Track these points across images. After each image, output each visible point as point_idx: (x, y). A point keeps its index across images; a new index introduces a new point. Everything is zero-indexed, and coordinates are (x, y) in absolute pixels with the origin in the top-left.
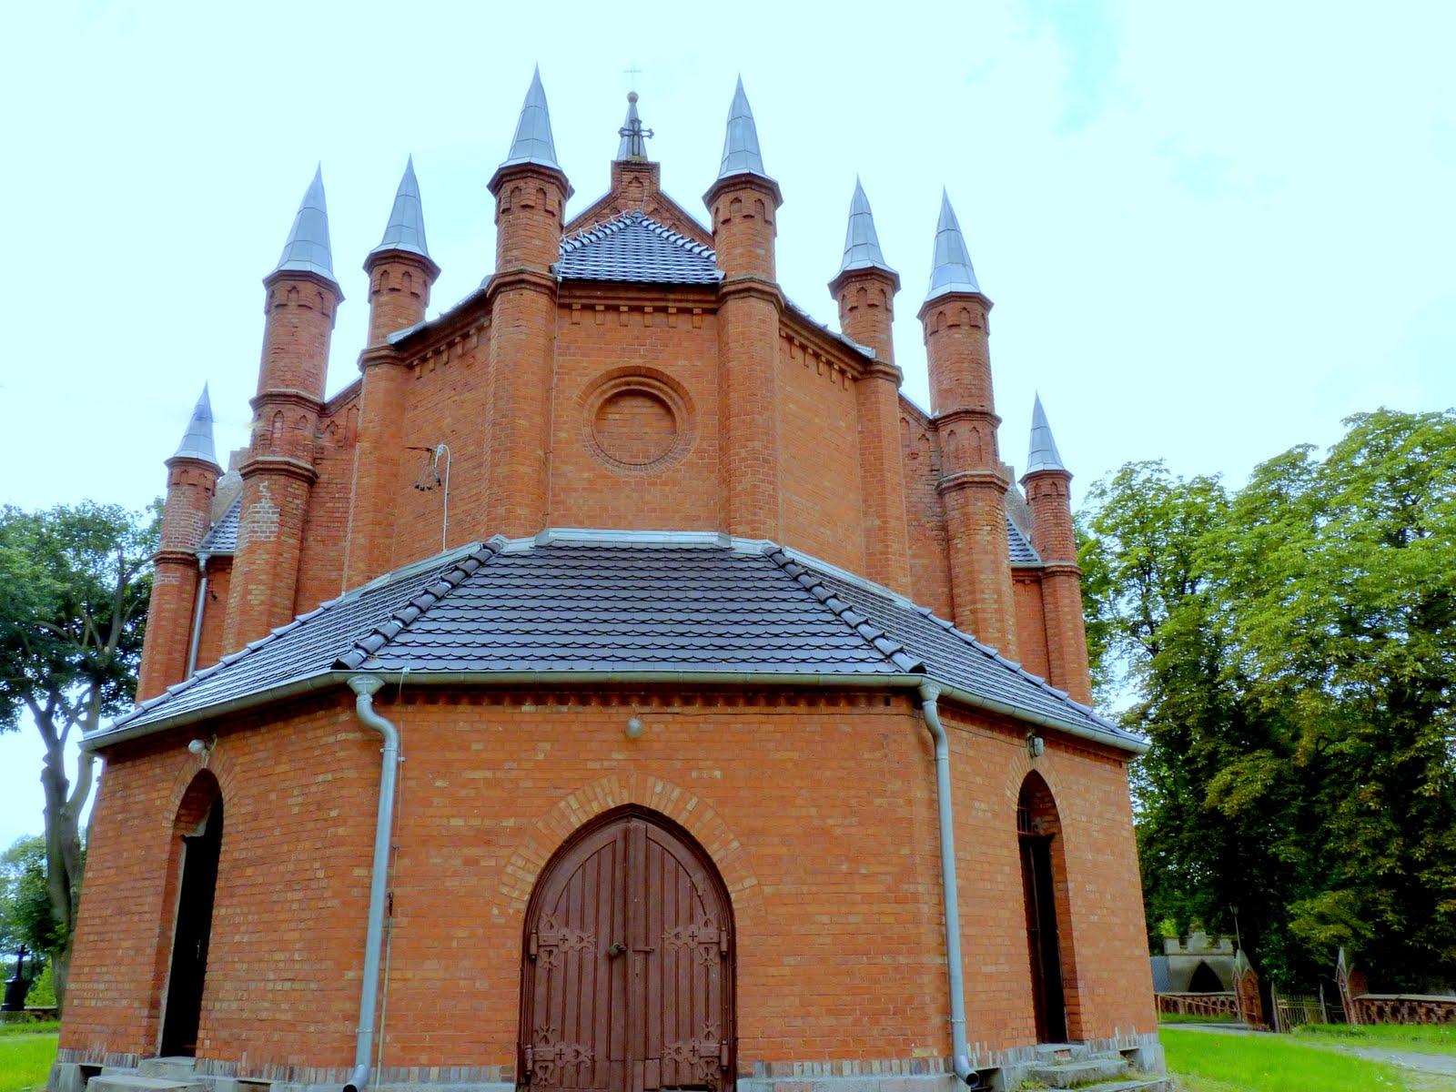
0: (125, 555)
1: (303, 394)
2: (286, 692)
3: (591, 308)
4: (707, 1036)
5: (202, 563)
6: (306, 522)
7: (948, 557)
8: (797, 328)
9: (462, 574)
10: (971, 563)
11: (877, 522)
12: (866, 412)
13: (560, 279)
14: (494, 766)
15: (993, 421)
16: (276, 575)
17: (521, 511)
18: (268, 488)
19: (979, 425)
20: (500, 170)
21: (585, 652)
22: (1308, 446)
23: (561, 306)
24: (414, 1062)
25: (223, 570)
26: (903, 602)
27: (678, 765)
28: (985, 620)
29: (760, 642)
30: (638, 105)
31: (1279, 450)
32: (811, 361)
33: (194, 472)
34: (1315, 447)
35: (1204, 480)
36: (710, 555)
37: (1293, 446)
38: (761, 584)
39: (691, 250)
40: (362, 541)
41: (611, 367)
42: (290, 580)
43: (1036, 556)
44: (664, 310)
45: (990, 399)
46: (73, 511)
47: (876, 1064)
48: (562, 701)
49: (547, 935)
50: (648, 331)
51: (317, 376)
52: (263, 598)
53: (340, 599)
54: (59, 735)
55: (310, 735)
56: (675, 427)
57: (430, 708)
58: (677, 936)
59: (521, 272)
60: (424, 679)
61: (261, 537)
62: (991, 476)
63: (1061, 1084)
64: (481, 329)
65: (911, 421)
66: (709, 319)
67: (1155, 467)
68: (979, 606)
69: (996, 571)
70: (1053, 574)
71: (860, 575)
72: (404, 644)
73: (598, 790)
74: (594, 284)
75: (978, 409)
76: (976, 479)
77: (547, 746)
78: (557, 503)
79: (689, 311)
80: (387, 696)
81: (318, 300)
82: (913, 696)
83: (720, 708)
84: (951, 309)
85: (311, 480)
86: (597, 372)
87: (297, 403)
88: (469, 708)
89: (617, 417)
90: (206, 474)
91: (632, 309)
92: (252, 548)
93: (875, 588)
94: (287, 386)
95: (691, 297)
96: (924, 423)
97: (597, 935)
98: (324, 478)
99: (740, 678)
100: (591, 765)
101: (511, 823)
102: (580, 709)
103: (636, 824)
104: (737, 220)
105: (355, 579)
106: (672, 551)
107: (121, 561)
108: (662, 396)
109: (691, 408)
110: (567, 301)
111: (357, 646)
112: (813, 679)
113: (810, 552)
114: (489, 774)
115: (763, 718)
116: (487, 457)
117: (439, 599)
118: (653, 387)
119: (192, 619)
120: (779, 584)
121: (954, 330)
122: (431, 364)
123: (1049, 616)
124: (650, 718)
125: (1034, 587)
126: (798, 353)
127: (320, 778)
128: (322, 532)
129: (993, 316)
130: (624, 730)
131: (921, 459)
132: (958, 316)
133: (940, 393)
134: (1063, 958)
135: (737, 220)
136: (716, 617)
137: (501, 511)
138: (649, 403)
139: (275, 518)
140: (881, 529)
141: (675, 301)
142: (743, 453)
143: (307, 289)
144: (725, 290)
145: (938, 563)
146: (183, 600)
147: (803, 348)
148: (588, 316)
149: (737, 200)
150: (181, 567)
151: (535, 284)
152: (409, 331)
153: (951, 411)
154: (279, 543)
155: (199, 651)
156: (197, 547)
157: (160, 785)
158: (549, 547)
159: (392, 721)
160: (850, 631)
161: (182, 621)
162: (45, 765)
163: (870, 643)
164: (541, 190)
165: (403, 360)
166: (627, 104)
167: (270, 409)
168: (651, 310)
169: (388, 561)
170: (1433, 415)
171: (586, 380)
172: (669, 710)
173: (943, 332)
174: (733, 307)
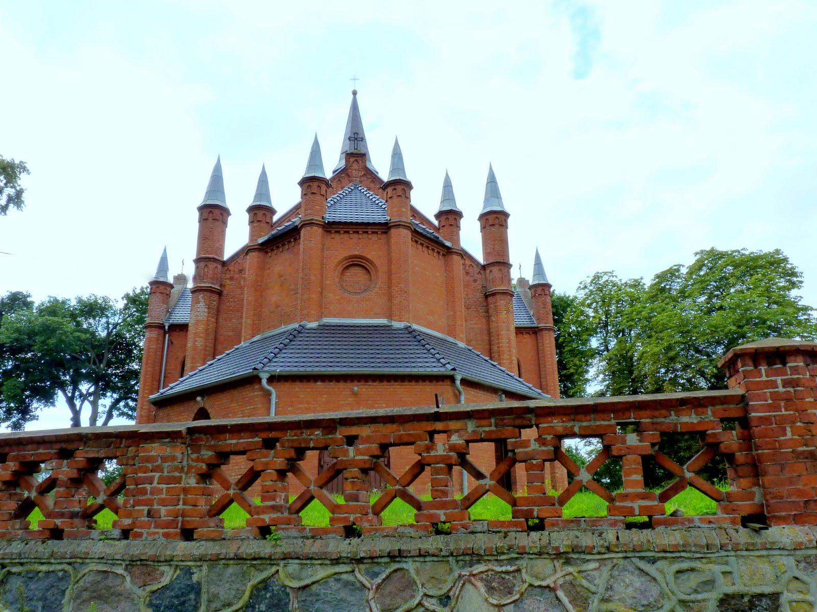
0: (110, 320)
1: (216, 257)
2: (237, 378)
3: (339, 232)
5: (167, 328)
6: (218, 311)
7: (489, 324)
8: (419, 237)
9: (294, 335)
10: (498, 327)
12: (448, 267)
13: (327, 222)
14: (308, 403)
15: (509, 266)
19: (502, 268)
20: (303, 178)
21: (338, 364)
22: (680, 265)
28: (503, 351)
31: (666, 268)
34: (683, 266)
35: (635, 281)
36: (384, 328)
37: (672, 265)
39: (378, 204)
41: (346, 255)
42: (212, 336)
43: (535, 322)
44: (367, 232)
45: (508, 256)
50: (360, 241)
54: (78, 408)
55: (244, 393)
57: (286, 383)
59: (312, 220)
60: (284, 374)
61: (201, 318)
62: (506, 290)
64: (295, 239)
66: (384, 236)
67: (610, 274)
69: (508, 330)
72: (276, 362)
74: (340, 223)
75: (502, 261)
77: (326, 396)
78: (326, 308)
79: (377, 233)
80: (272, 379)
81: (221, 217)
82: (452, 379)
84: (491, 218)
85: (220, 293)
87: (214, 262)
88: (299, 383)
90: (167, 288)
91: (354, 232)
93: (451, 339)
94: (209, 254)
95: (377, 227)
96: (480, 267)
98: (225, 292)
99: (391, 373)
100: (341, 402)
102: (337, 383)
104: (395, 197)
106: (370, 327)
107: (108, 323)
108: (365, 266)
109: (377, 271)
110: (329, 230)
111: (260, 363)
112: (417, 373)
113: (424, 326)
114: (307, 406)
115: (399, 387)
116: (300, 291)
117: (285, 345)
118: (362, 262)
121: (492, 227)
123: (541, 348)
125: (533, 336)
126: (420, 247)
127: (249, 408)
128: (225, 315)
129: (510, 221)
130: (352, 391)
131: (478, 282)
132: (495, 222)
135: (395, 197)
136: (385, 352)
138: (361, 269)
139: (206, 310)
141: (371, 229)
142: (396, 289)
143: (217, 212)
144: (390, 225)
146: (159, 344)
147: (422, 244)
149: (395, 189)
150: (157, 329)
151: (317, 224)
152: (266, 238)
153: (490, 262)
154: (208, 320)
156: (164, 320)
157: (183, 414)
158: (324, 326)
161: (158, 353)
162: (72, 423)
164: (319, 186)
165: (263, 250)
166: (352, 96)
167: (202, 264)
168: (361, 232)
169: (260, 330)
171: (336, 261)
174: (393, 231)
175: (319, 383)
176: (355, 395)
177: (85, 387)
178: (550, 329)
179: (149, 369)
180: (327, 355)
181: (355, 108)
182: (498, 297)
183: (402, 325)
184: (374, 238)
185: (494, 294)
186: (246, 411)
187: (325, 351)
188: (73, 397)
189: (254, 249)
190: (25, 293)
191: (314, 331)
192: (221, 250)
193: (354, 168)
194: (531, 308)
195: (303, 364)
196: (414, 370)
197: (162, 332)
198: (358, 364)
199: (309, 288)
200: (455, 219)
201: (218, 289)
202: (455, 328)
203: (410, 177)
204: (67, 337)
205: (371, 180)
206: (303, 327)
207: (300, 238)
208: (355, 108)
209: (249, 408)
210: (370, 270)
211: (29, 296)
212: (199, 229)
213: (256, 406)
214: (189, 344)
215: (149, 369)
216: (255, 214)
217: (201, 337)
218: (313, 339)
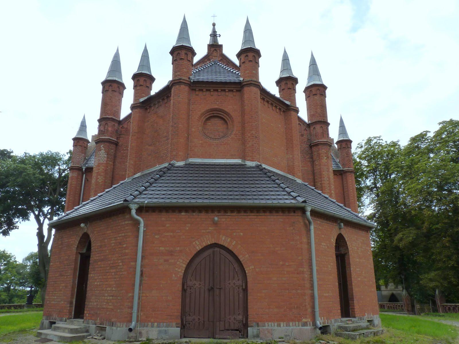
3: (202, 90)
4: (239, 314)
5: (84, 170)
6: (115, 157)
7: (313, 167)
8: (266, 95)
9: (163, 173)
11: (291, 156)
13: (192, 81)
17: (180, 153)
18: (103, 147)
22: (427, 132)
23: (192, 90)
24: (149, 321)
26: (299, 181)
29: (255, 193)
30: (216, 27)
31: (418, 133)
34: (429, 132)
35: (394, 143)
38: (255, 175)
43: (341, 166)
44: (224, 90)
45: (326, 117)
46: (45, 154)
47: (291, 324)
48: (193, 211)
49: (189, 283)
52: (102, 180)
53: (125, 180)
54: (42, 222)
56: (226, 122)
57: (154, 214)
58: (229, 283)
59: (180, 79)
63: (349, 330)
66: (238, 93)
67: (378, 138)
68: (323, 182)
69: (328, 171)
71: (286, 173)
73: (205, 239)
75: (323, 120)
76: (322, 143)
77: (189, 225)
79: (232, 91)
81: (118, 89)
82: (303, 210)
84: (313, 89)
85: (116, 144)
86: (203, 111)
87: (112, 121)
89: (210, 124)
92: (98, 166)
96: (306, 125)
97: (205, 283)
98: (120, 143)
100: (203, 231)
101: (178, 249)
103: (217, 249)
104: (247, 62)
107: (59, 169)
108: (224, 117)
109: (233, 121)
110: (194, 88)
111: (131, 195)
114: (172, 234)
115: (255, 217)
116: (170, 136)
117: (156, 180)
119: (81, 186)
126: (266, 104)
127: (120, 235)
129: (327, 92)
130: (213, 220)
132: (317, 92)
135: (247, 62)
139: (106, 156)
143: (115, 85)
147: (268, 102)
149: (247, 56)
153: (314, 121)
154: (107, 163)
158: (189, 164)
159: (142, 218)
160: (282, 190)
162: (37, 231)
163: (289, 194)
166: (212, 27)
167: (103, 123)
172: (227, 214)
174: (246, 89)
175: (183, 214)
176: (215, 224)
177: (46, 209)
179: (71, 198)
180: (168, 185)
182: (320, 147)
183: (254, 164)
184: (230, 94)
186: (118, 238)
187: (189, 185)
188: (39, 215)
190: (9, 151)
191: (180, 169)
192: (119, 116)
193: (213, 55)
194: (337, 158)
195: (170, 196)
196: (256, 201)
197: (80, 173)
198: (218, 197)
199: (177, 134)
200: (292, 84)
201: (115, 141)
202: (294, 168)
204: (29, 177)
205: (226, 63)
206: (172, 165)
207: (171, 96)
209: (120, 235)
210: (228, 122)
211: (12, 152)
212: (103, 98)
213: (126, 234)
214: (93, 181)
215: (71, 198)
216: (138, 80)
217: (101, 176)
218: (180, 175)
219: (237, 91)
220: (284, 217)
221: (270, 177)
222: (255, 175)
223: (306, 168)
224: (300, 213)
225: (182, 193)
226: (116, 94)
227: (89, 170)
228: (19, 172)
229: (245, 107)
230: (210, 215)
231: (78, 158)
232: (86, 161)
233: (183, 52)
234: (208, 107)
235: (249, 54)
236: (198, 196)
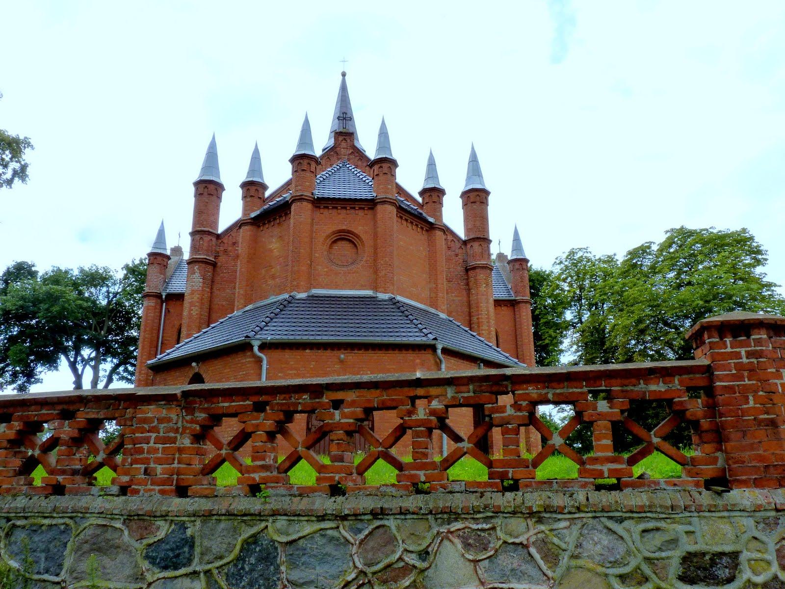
0: (110, 289)
1: (211, 230)
5: (164, 297)
9: (285, 305)
11: (434, 286)
13: (316, 197)
16: (202, 304)
17: (302, 283)
18: (198, 269)
20: (294, 156)
21: (325, 333)
22: (651, 243)
23: (317, 207)
25: (178, 303)
26: (443, 316)
27: (356, 369)
28: (482, 322)
29: (384, 330)
32: (409, 225)
33: (159, 258)
34: (654, 243)
35: (609, 257)
38: (386, 310)
39: (365, 181)
40: (242, 292)
42: (207, 306)
43: (513, 295)
44: (354, 208)
45: (488, 232)
46: (88, 270)
48: (319, 349)
51: (215, 223)
52: (197, 312)
53: (234, 314)
54: (80, 372)
56: (355, 246)
59: (302, 195)
62: (486, 264)
65: (456, 241)
66: (370, 212)
67: (585, 251)
69: (487, 302)
70: (519, 302)
71: (427, 306)
72: (267, 330)
75: (482, 237)
77: (313, 363)
79: (363, 209)
80: (264, 347)
81: (215, 192)
82: (433, 348)
83: (370, 351)
84: (472, 195)
85: (214, 265)
86: (330, 231)
87: (209, 235)
91: (342, 208)
92: (193, 292)
93: (433, 310)
94: (204, 227)
98: (219, 264)
99: (376, 342)
105: (240, 306)
107: (108, 292)
109: (363, 245)
111: (252, 331)
113: (407, 297)
118: (349, 237)
119: (160, 320)
120: (393, 310)
121: (473, 204)
122: (267, 226)
124: (348, 354)
125: (512, 308)
126: (404, 223)
127: (241, 373)
130: (339, 358)
132: (476, 199)
133: (468, 230)
134: (489, 439)
136: (370, 322)
137: (295, 283)
138: (348, 243)
139: (201, 280)
140: (435, 288)
141: (358, 205)
143: (212, 187)
144: (377, 201)
145: (465, 299)
147: (406, 220)
148: (326, 210)
149: (381, 167)
153: (471, 238)
155: (163, 333)
157: (179, 378)
158: (313, 296)
160: (415, 326)
167: (197, 237)
170: (704, 230)
173: (469, 204)
174: (379, 207)
175: (307, 351)
176: (341, 362)
178: (526, 302)
181: (344, 88)
182: (477, 270)
185: (474, 268)
189: (248, 223)
190: (30, 263)
199: (298, 261)
203: (395, 155)
205: (358, 158)
206: (293, 297)
207: (290, 213)
208: (344, 88)
213: (248, 372)
214: (185, 313)
217: (195, 306)
219: (369, 209)
220: (414, 355)
221: (403, 312)
222: (386, 310)
223: (459, 298)
224: (430, 352)
225: (307, 329)
226: (214, 198)
227: (180, 297)
228: (52, 298)
229: (378, 229)
230: (335, 352)
231: (155, 280)
232: (165, 284)
233: (305, 162)
234: (335, 228)
235: (383, 165)
236: (330, 325)
